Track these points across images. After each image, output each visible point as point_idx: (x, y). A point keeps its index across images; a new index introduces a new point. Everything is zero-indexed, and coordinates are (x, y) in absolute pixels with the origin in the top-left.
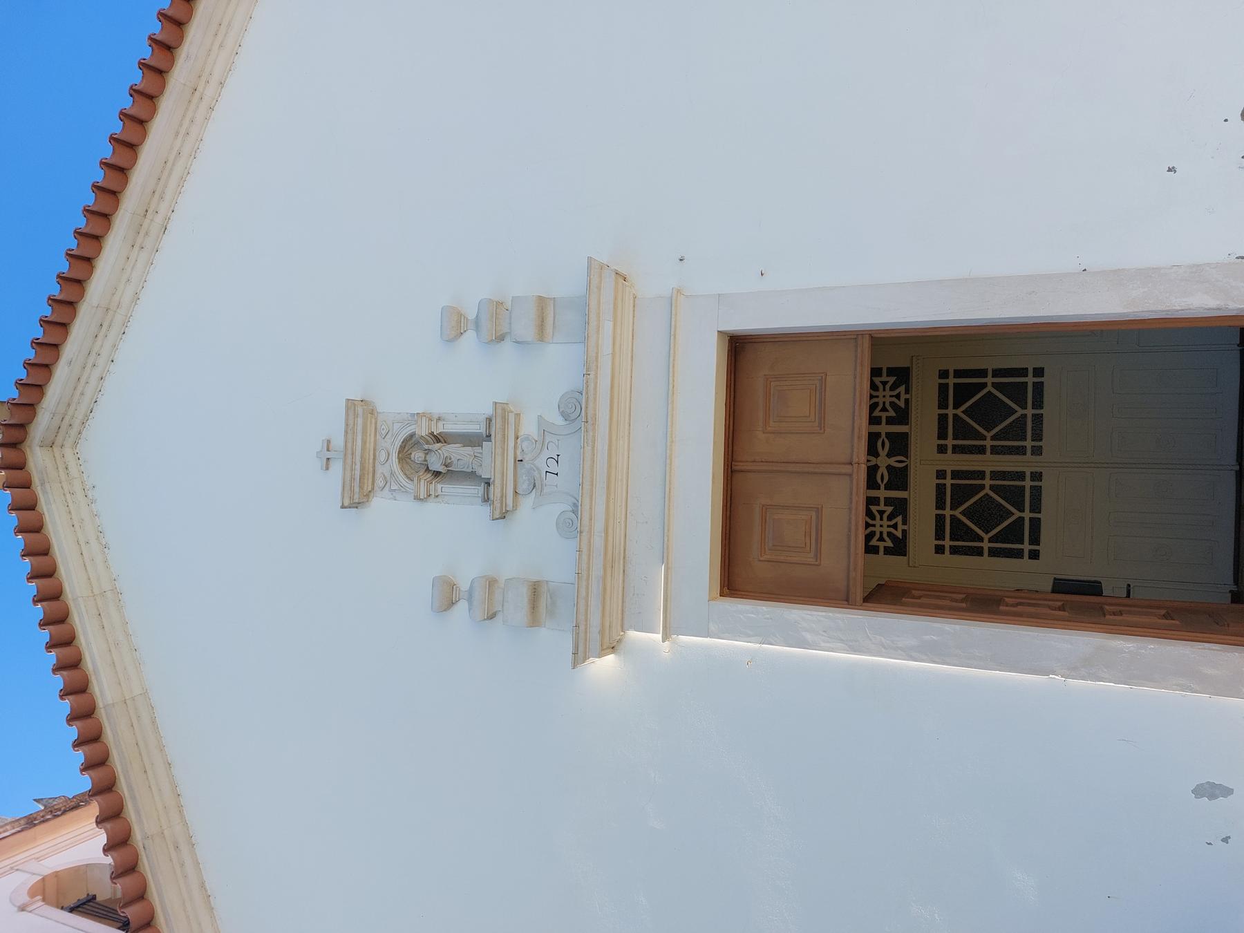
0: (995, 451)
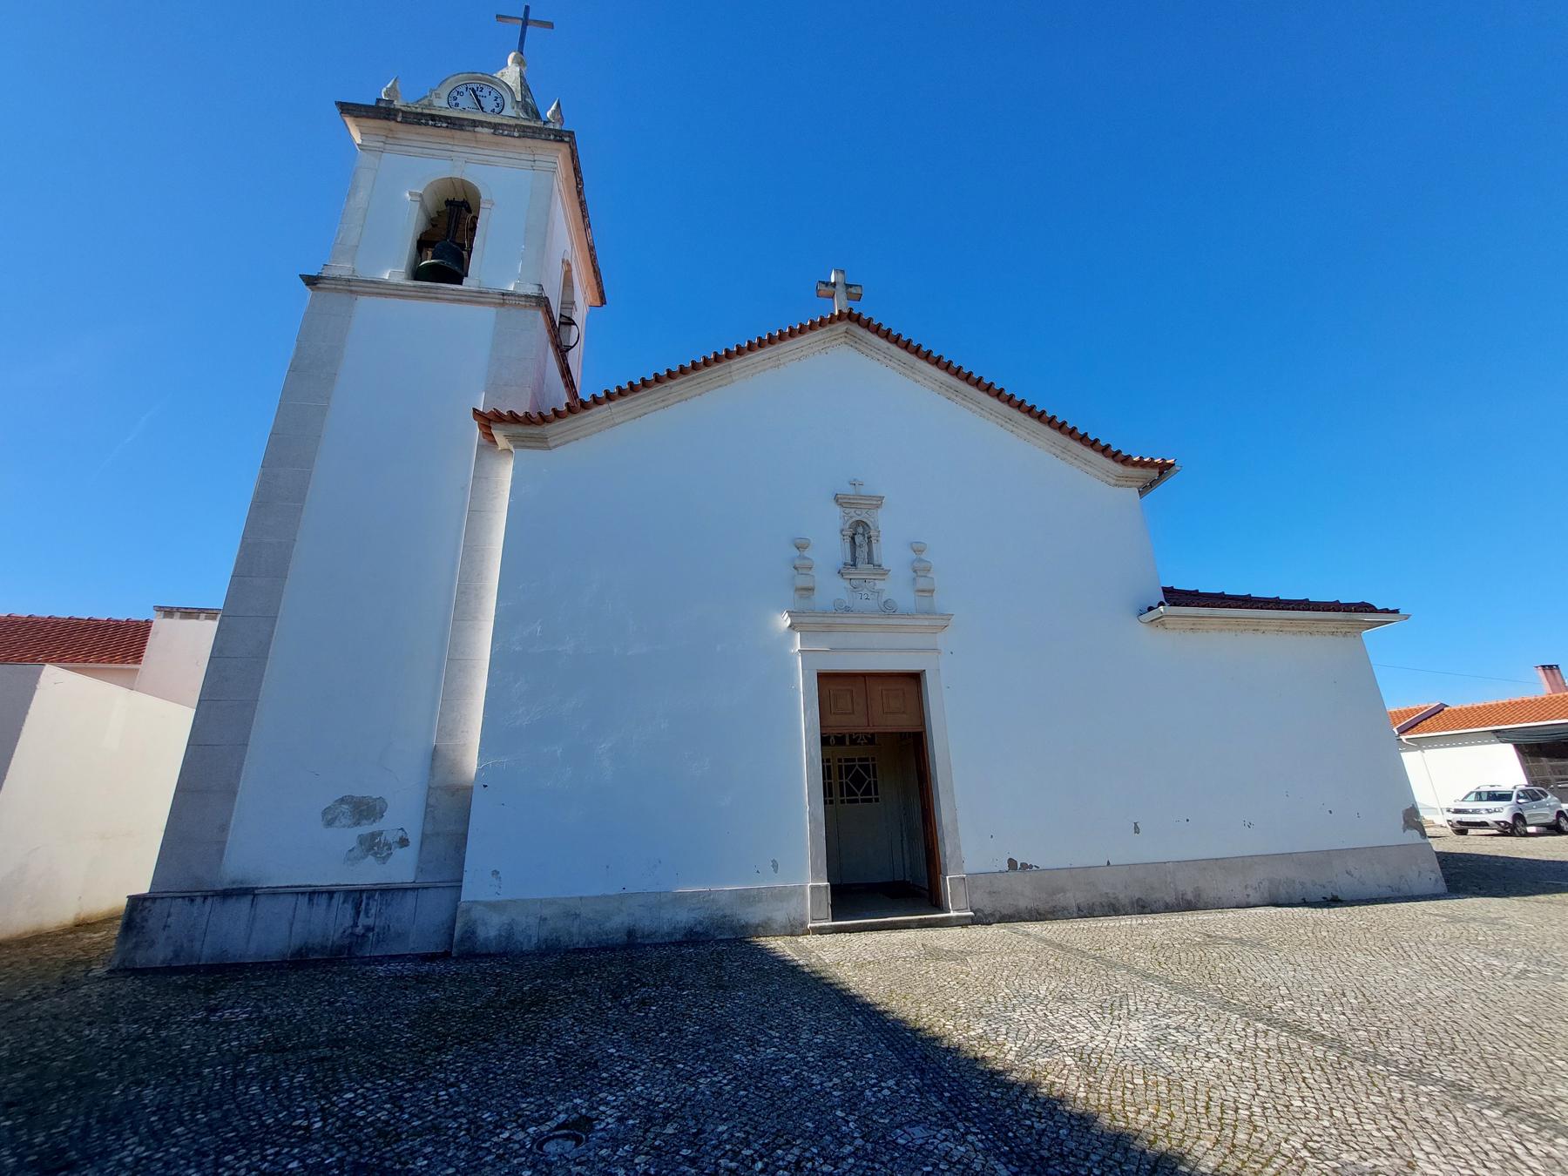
0: (841, 784)
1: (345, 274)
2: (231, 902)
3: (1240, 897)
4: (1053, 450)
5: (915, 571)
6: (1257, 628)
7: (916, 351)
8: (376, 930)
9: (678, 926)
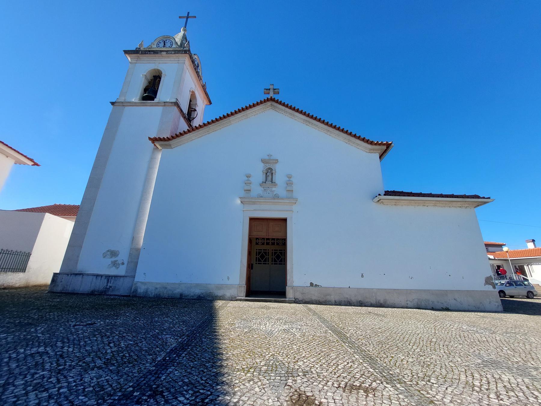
0: (272, 258)
1: (122, 101)
2: (77, 276)
3: (403, 303)
4: (345, 141)
5: (287, 184)
6: (424, 204)
7: (294, 109)
8: (112, 287)
9: (196, 294)
